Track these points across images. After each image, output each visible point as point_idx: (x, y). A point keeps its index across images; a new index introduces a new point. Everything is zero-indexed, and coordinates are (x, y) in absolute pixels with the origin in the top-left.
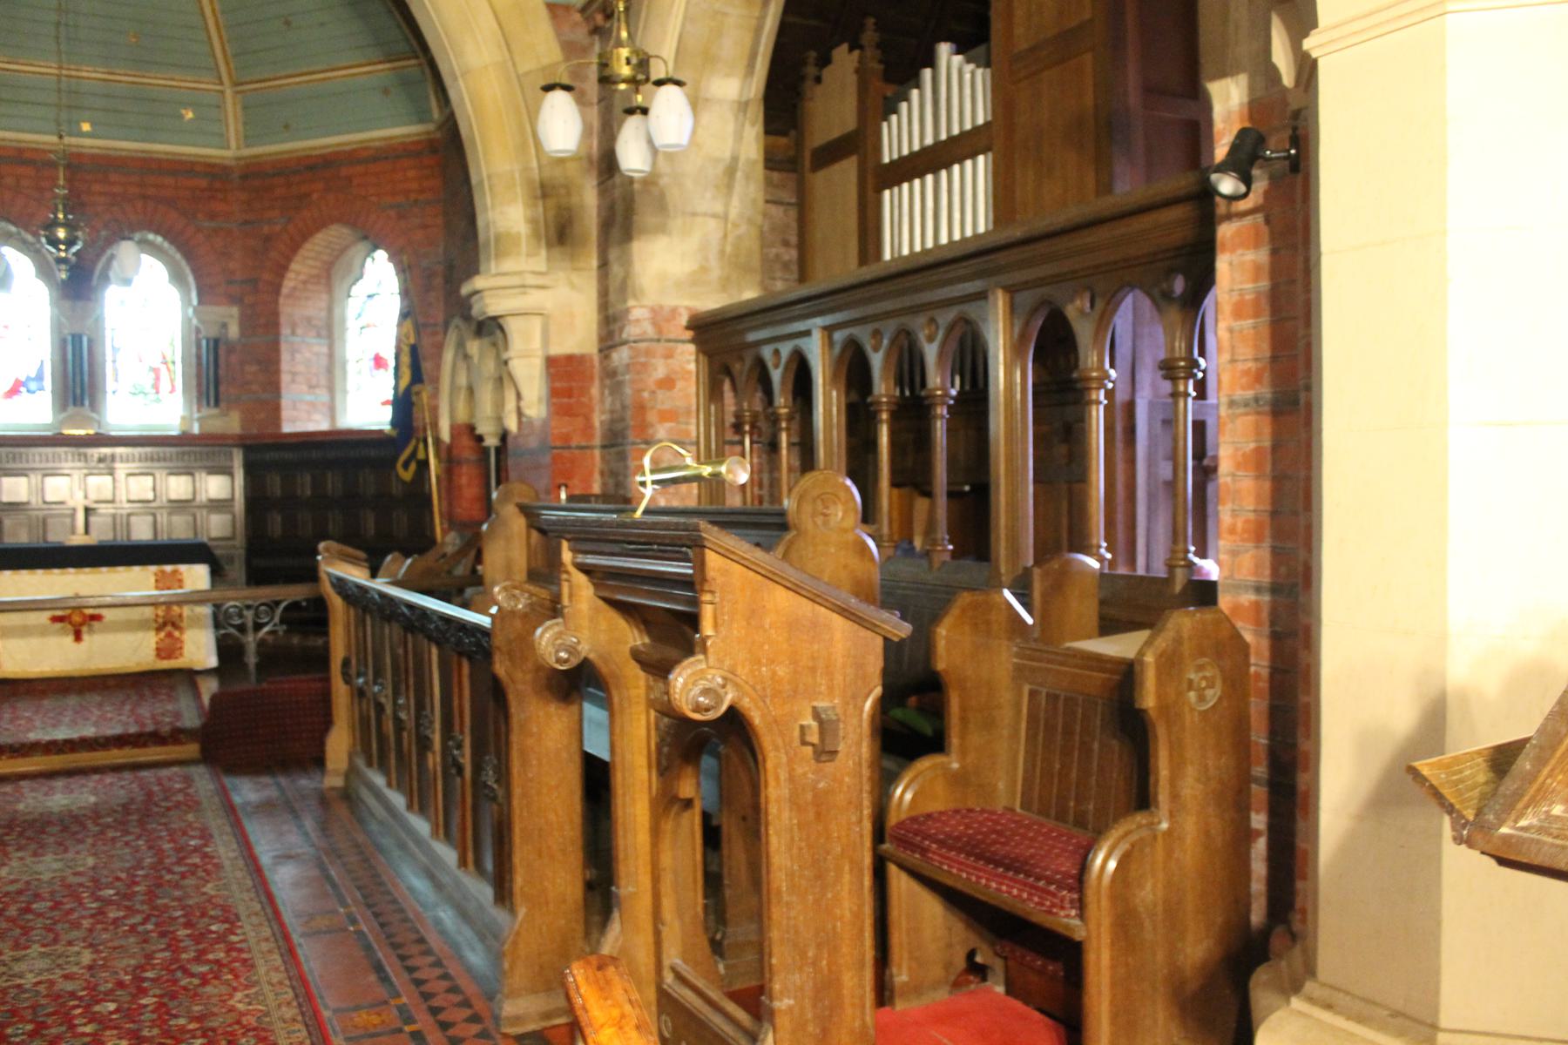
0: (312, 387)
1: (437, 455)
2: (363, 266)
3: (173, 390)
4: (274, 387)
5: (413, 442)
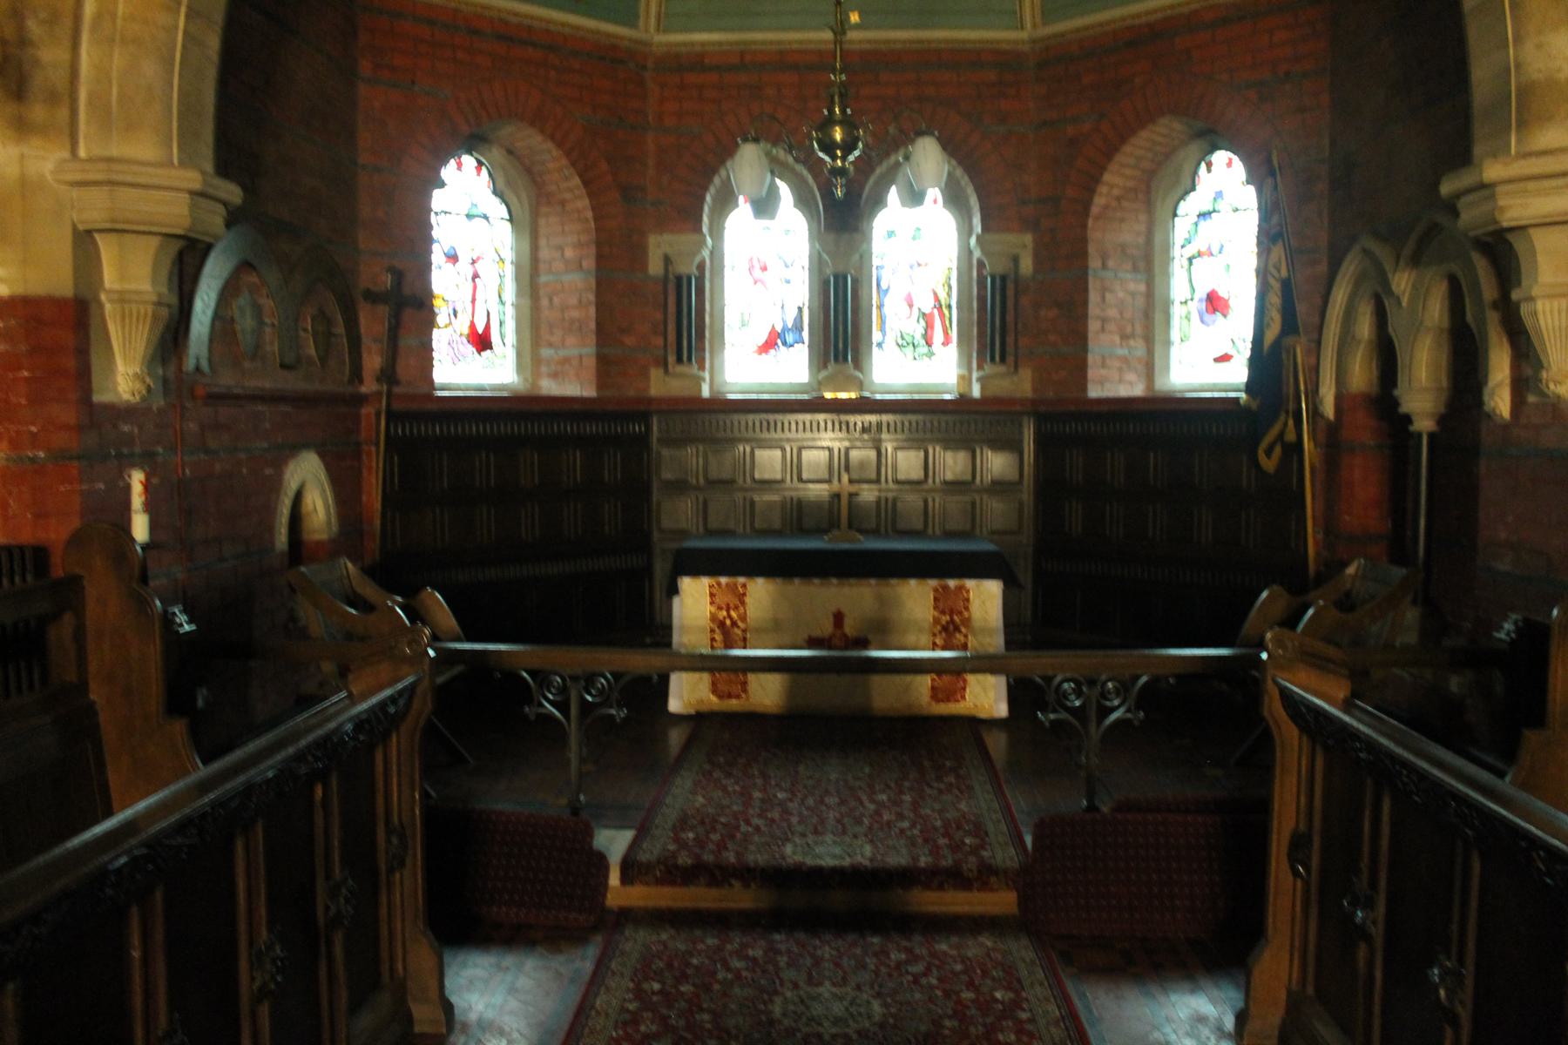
0: (1125, 337)
1: (1313, 436)
2: (1195, 173)
3: (946, 343)
4: (1080, 339)
5: (1282, 417)
